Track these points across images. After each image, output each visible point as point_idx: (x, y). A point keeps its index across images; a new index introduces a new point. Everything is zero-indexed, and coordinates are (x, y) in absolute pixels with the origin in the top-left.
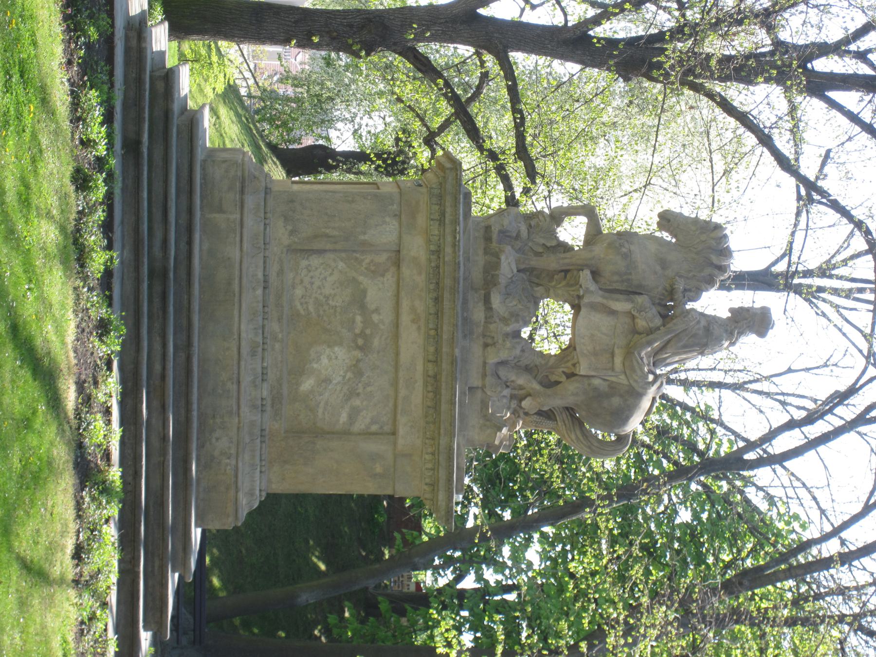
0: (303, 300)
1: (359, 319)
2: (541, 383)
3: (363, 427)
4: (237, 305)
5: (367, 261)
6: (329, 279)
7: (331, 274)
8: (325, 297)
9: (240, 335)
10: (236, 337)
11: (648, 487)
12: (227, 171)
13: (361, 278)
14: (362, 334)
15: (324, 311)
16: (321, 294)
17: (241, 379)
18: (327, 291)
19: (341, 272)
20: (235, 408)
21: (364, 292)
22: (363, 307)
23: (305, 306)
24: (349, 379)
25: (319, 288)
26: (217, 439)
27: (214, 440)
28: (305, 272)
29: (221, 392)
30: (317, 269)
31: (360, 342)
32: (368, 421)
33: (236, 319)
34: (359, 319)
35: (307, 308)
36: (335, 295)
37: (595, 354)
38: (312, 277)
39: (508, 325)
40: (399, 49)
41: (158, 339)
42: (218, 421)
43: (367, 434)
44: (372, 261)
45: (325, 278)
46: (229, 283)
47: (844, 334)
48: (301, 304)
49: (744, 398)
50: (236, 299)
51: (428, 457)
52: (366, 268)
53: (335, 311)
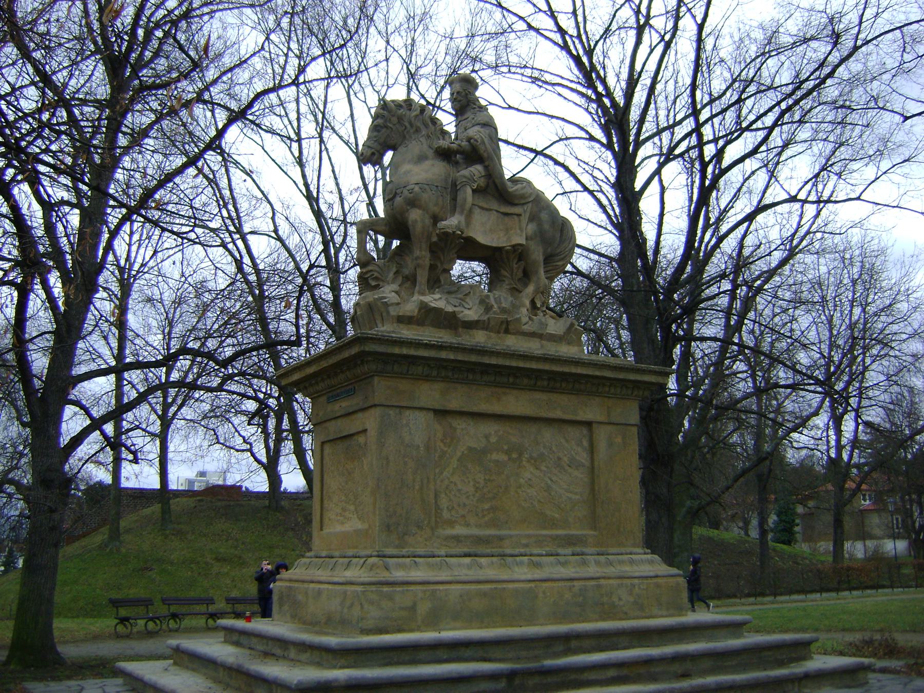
0: (480, 515)
1: (495, 456)
2: (526, 285)
3: (585, 455)
4: (505, 586)
5: (442, 445)
6: (460, 487)
7: (455, 484)
8: (476, 491)
9: (530, 581)
10: (533, 585)
11: (261, 392)
12: (372, 603)
13: (459, 454)
14: (508, 452)
15: (489, 492)
16: (474, 495)
17: (568, 577)
18: (471, 490)
19: (452, 474)
20: (593, 583)
21: (470, 449)
22: (485, 451)
23: (485, 513)
24: (547, 467)
25: (468, 497)
26: (620, 599)
27: (621, 603)
28: (453, 513)
29: (581, 598)
30: (450, 500)
31: (514, 456)
32: (580, 449)
33: (516, 585)
34: (495, 456)
35: (488, 510)
36: (474, 480)
37: (507, 230)
38: (459, 505)
39: (492, 306)
40: (343, 331)
41: (586, 675)
42: (605, 599)
43: (592, 450)
44: (442, 441)
45: (459, 491)
46: (484, 594)
47: (286, 173)
48: (484, 516)
49: (559, 94)
50: (499, 586)
51: (612, 390)
52: (449, 446)
53: (489, 480)
